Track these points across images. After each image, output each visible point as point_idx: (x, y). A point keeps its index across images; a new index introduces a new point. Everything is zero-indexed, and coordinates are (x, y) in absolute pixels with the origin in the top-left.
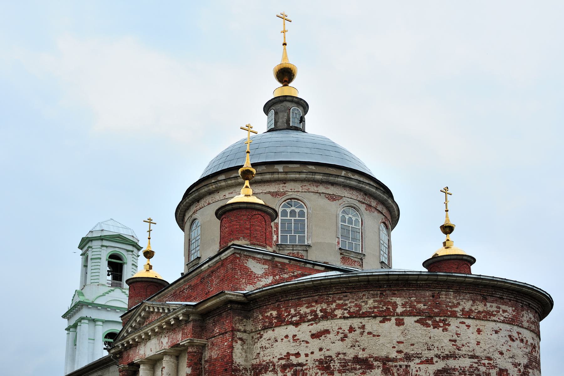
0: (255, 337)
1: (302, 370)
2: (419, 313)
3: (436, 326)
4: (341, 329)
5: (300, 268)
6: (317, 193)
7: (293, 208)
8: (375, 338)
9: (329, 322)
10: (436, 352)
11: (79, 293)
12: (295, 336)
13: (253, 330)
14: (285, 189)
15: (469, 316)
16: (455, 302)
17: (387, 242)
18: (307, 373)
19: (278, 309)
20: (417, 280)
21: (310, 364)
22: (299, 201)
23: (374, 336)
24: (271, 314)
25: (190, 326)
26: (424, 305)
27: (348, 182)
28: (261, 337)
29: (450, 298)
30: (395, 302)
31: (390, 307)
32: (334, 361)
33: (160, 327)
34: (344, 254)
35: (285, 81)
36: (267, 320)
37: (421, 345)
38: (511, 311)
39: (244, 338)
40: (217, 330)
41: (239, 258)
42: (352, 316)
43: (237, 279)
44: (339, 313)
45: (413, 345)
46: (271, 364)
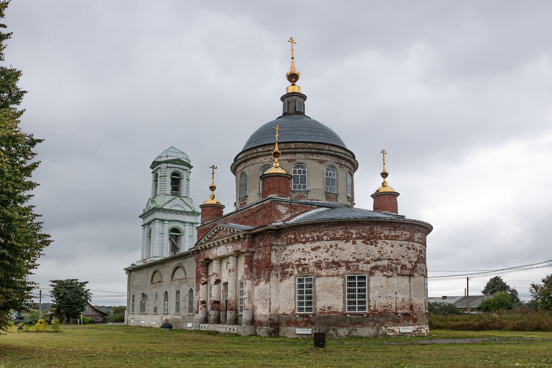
0: (282, 249)
1: (307, 267)
2: (364, 237)
3: (371, 244)
4: (326, 246)
5: (305, 207)
6: (313, 159)
7: (300, 169)
8: (342, 251)
9: (320, 242)
10: (371, 258)
11: (152, 201)
12: (303, 249)
13: (281, 245)
14: (296, 158)
15: (387, 238)
16: (381, 231)
17: (351, 183)
18: (309, 269)
19: (295, 234)
20: (362, 221)
21: (311, 264)
22: (303, 165)
23: (342, 250)
24: (291, 237)
25: (246, 241)
26: (366, 234)
27: (330, 152)
28: (286, 249)
29: (378, 230)
30: (352, 232)
31: (349, 235)
32: (323, 263)
33: (228, 240)
34: (327, 194)
35: (293, 81)
36: (289, 240)
37: (364, 254)
38: (409, 234)
39: (277, 249)
40: (262, 244)
41: (274, 205)
42: (332, 239)
43: (273, 217)
44: (325, 237)
45: (360, 254)
46: (291, 264)
